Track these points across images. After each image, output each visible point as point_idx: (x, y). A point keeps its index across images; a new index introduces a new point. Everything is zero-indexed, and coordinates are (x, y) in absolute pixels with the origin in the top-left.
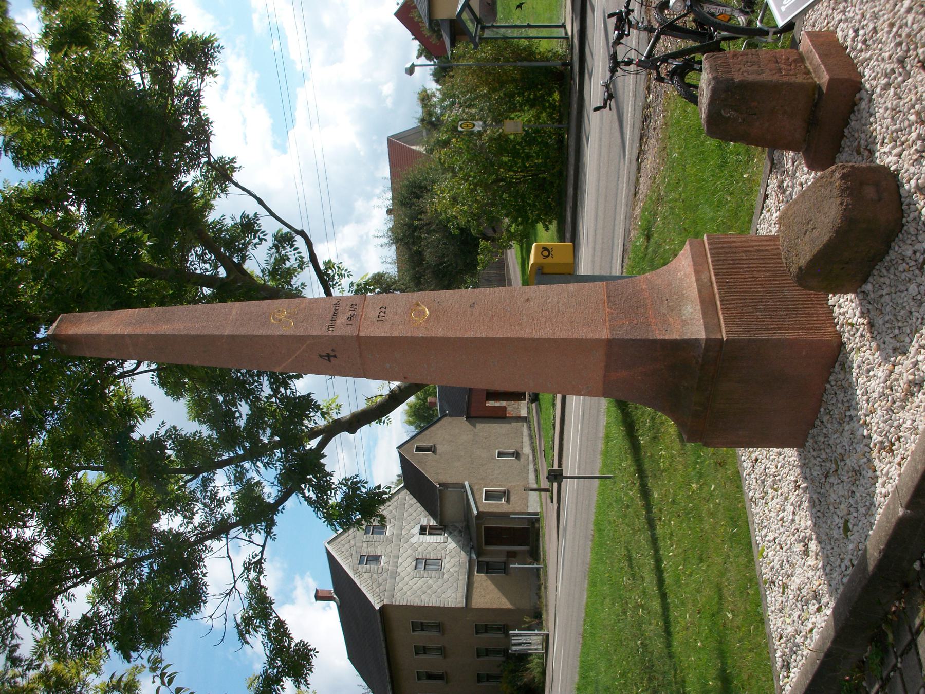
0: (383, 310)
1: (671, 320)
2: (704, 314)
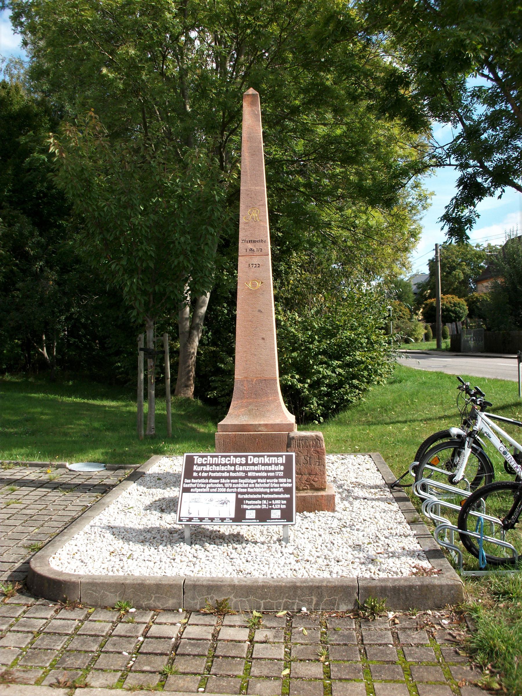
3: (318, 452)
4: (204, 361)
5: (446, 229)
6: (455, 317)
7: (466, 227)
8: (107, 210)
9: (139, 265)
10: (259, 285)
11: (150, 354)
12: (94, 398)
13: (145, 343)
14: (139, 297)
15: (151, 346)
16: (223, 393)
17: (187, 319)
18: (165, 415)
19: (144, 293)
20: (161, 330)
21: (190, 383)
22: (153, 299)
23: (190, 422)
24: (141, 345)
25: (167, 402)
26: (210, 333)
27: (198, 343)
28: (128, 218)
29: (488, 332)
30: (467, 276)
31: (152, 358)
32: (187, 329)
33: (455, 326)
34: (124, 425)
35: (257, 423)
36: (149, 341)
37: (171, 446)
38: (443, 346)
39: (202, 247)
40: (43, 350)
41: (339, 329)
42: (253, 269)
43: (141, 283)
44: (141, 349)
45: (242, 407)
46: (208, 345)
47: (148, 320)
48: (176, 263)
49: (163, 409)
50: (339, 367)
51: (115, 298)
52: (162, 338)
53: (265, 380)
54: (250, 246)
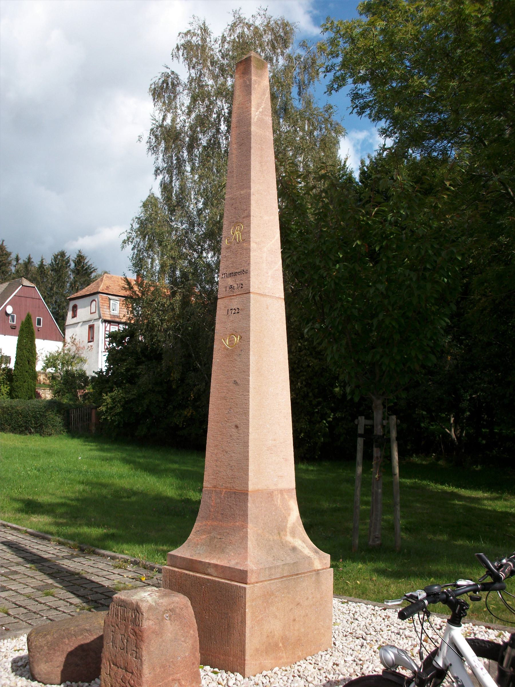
1: (204, 537)
10: (236, 340)
40: (450, 431)
42: (232, 317)
53: (235, 493)
54: (230, 281)
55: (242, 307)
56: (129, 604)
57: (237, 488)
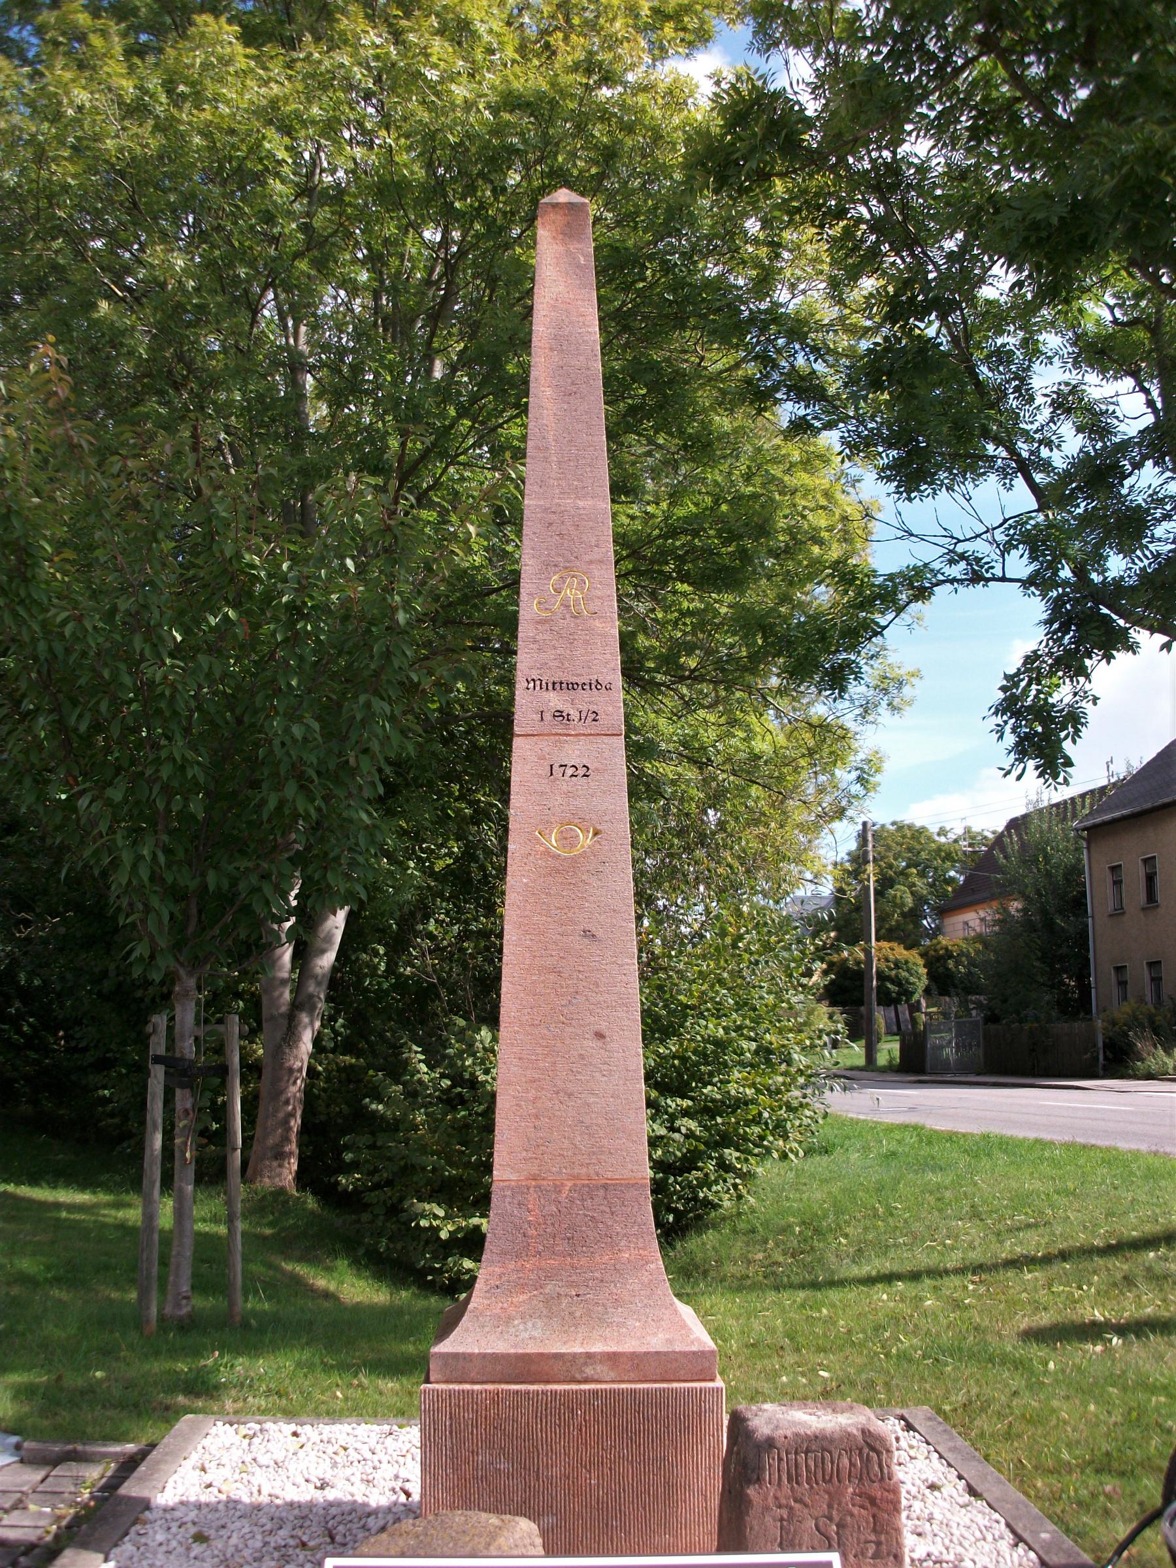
0: (581, 771)
1: (522, 1298)
2: (496, 1358)
3: (873, 1501)
4: (324, 1090)
5: (1010, 739)
6: (898, 993)
7: (1063, 735)
8: (73, 634)
9: (161, 805)
11: (184, 1073)
12: (34, 1181)
13: (171, 1046)
14: (155, 902)
15: (188, 1049)
16: (376, 1178)
17: (284, 982)
18: (220, 1238)
19: (177, 894)
20: (215, 1006)
21: (287, 1149)
22: (200, 912)
23: (288, 1258)
24: (158, 1046)
25: (229, 1203)
26: (341, 1021)
27: (310, 1047)
28: (135, 663)
29: (992, 1027)
30: (920, 900)
31: (190, 1086)
32: (284, 1009)
33: (893, 1014)
34: (107, 1267)
35: (578, 1349)
36: (182, 1036)
37: (241, 1365)
38: (882, 1059)
39: (352, 761)
41: (686, 1016)
42: (565, 784)
43: (162, 859)
44: (158, 1060)
45: (522, 1287)
46: (333, 1051)
47: (182, 972)
48: (272, 804)
49: (215, 1219)
50: (686, 1113)
51: (99, 927)
52: (221, 1028)
53: (605, 1187)
54: (555, 700)
55: (596, 765)
56: (841, 1439)
57: (609, 1175)
